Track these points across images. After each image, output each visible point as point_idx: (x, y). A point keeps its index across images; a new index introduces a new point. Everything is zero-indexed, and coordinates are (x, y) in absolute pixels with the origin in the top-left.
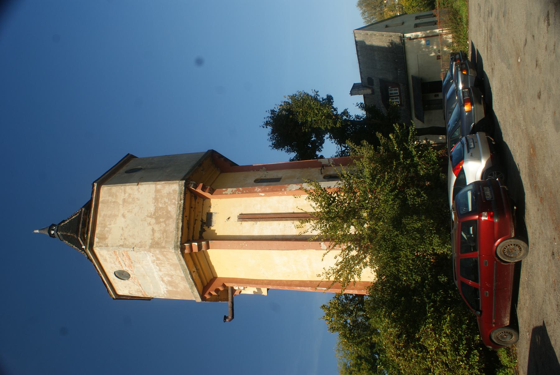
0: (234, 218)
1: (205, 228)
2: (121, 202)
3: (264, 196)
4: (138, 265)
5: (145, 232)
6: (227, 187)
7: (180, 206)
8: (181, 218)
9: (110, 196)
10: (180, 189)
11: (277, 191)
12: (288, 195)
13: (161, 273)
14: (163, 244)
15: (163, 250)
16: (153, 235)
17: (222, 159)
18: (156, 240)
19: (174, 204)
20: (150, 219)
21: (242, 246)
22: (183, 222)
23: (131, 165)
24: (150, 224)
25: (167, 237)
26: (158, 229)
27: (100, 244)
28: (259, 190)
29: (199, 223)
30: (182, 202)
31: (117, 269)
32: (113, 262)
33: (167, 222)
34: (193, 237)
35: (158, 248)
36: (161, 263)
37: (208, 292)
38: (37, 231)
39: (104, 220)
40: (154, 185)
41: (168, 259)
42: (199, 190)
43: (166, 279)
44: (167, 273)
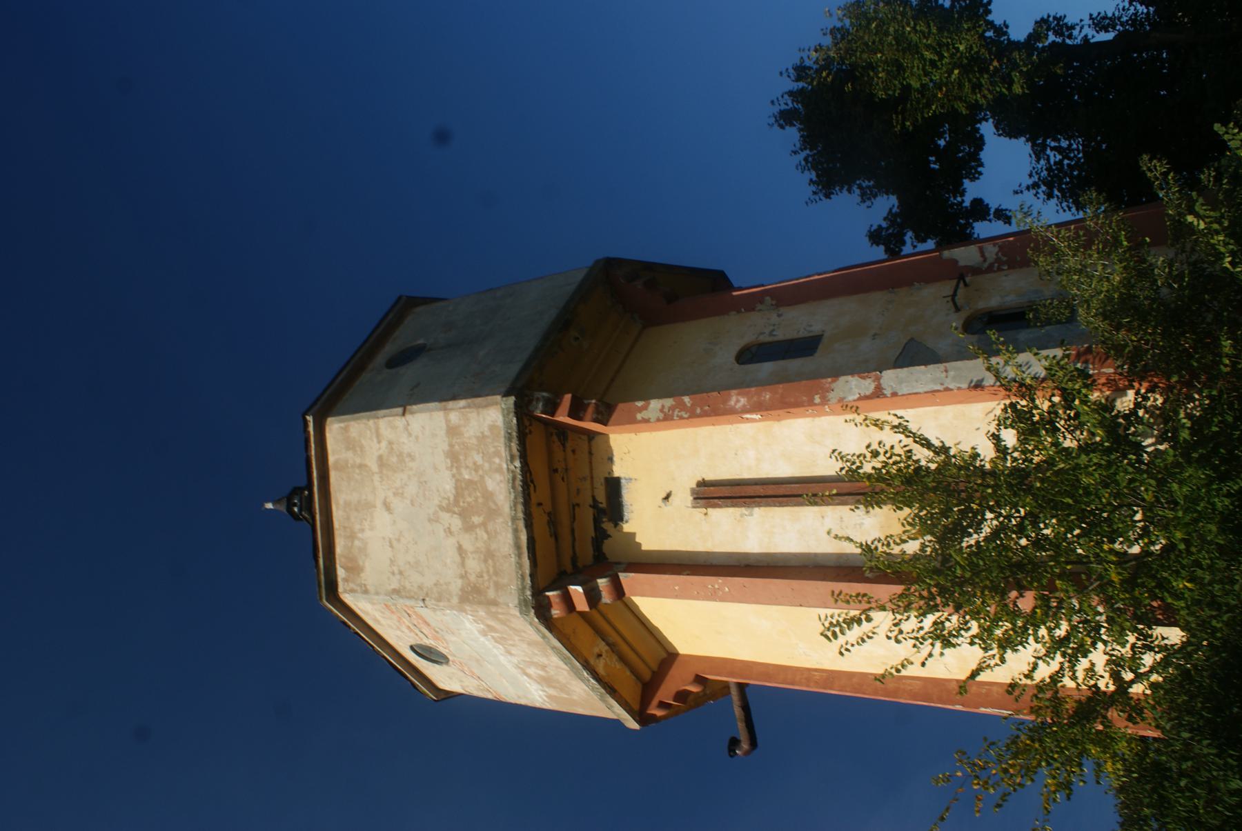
0: (683, 497)
1: (608, 526)
2: (374, 467)
3: (760, 420)
6: (647, 397)
7: (514, 479)
8: (521, 515)
9: (348, 449)
10: (507, 424)
11: (797, 405)
12: (833, 413)
14: (491, 594)
15: (493, 609)
16: (463, 564)
18: (473, 578)
19: (499, 470)
20: (448, 515)
21: (715, 591)
25: (496, 573)
27: (352, 585)
28: (743, 401)
29: (588, 515)
30: (518, 464)
31: (413, 643)
34: (574, 559)
35: (480, 603)
37: (655, 702)
38: (269, 506)
39: (348, 518)
40: (441, 414)
42: (562, 417)
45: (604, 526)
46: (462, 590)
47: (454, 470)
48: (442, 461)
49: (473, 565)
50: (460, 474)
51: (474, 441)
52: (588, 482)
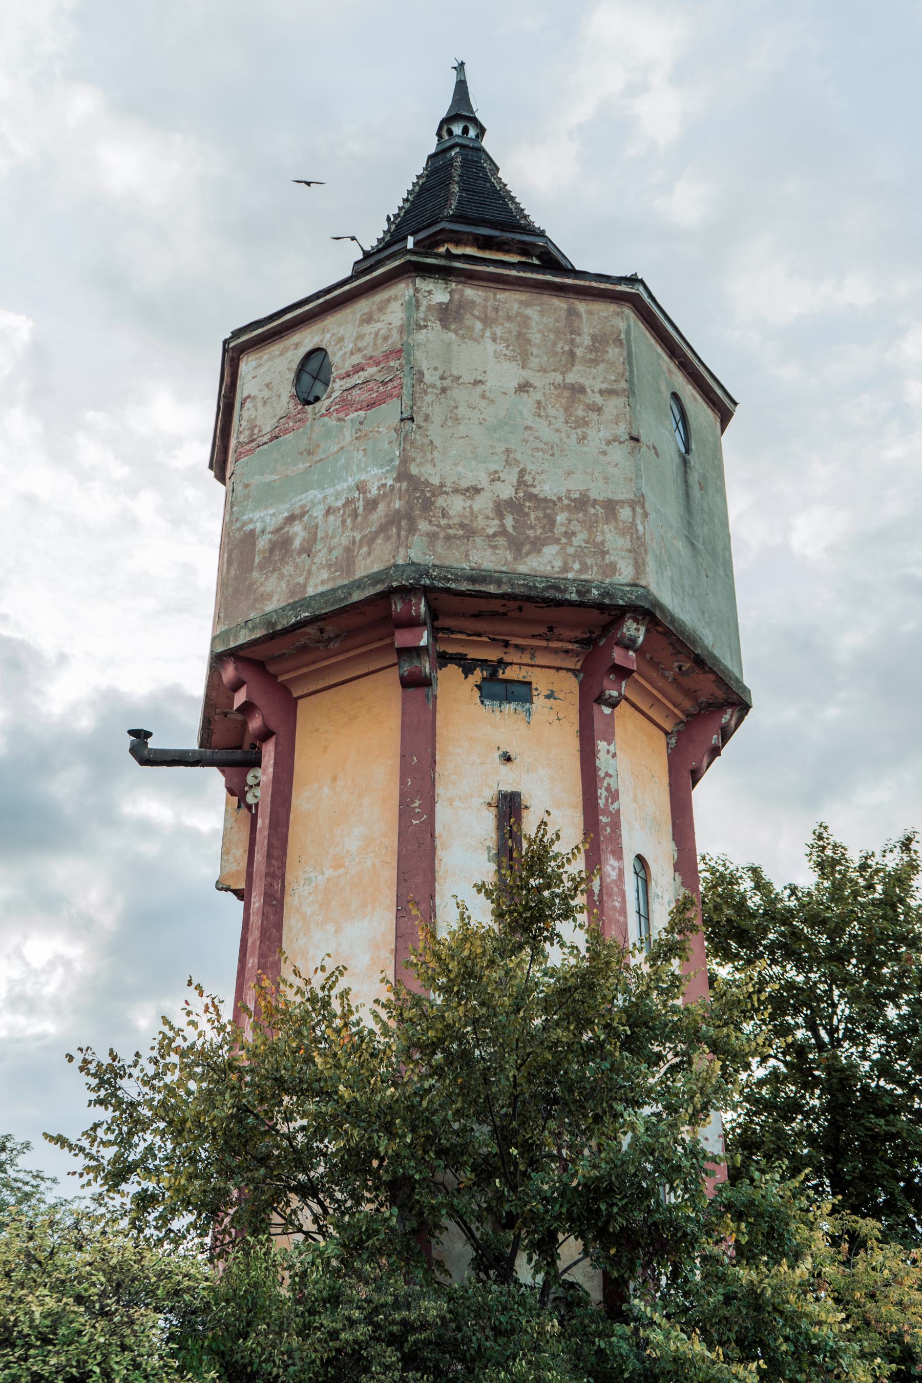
0: (508, 780)
2: (572, 377)
4: (348, 435)
5: (468, 462)
9: (594, 338)
13: (318, 513)
16: (456, 491)
17: (715, 739)
18: (440, 501)
19: (566, 568)
22: (503, 596)
23: (700, 412)
24: (495, 478)
25: (448, 538)
26: (476, 507)
29: (492, 655)
32: (361, 344)
33: (501, 541)
36: (355, 514)
37: (246, 675)
39: (509, 318)
41: (370, 540)
43: (297, 528)
44: (320, 535)
45: (478, 671)
46: (427, 483)
47: (566, 502)
48: (576, 485)
49: (457, 505)
50: (562, 510)
51: (599, 539)
52: (529, 661)
